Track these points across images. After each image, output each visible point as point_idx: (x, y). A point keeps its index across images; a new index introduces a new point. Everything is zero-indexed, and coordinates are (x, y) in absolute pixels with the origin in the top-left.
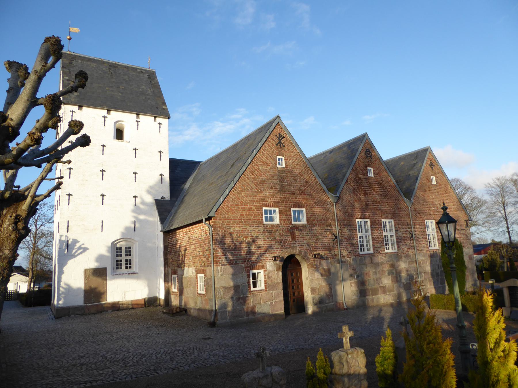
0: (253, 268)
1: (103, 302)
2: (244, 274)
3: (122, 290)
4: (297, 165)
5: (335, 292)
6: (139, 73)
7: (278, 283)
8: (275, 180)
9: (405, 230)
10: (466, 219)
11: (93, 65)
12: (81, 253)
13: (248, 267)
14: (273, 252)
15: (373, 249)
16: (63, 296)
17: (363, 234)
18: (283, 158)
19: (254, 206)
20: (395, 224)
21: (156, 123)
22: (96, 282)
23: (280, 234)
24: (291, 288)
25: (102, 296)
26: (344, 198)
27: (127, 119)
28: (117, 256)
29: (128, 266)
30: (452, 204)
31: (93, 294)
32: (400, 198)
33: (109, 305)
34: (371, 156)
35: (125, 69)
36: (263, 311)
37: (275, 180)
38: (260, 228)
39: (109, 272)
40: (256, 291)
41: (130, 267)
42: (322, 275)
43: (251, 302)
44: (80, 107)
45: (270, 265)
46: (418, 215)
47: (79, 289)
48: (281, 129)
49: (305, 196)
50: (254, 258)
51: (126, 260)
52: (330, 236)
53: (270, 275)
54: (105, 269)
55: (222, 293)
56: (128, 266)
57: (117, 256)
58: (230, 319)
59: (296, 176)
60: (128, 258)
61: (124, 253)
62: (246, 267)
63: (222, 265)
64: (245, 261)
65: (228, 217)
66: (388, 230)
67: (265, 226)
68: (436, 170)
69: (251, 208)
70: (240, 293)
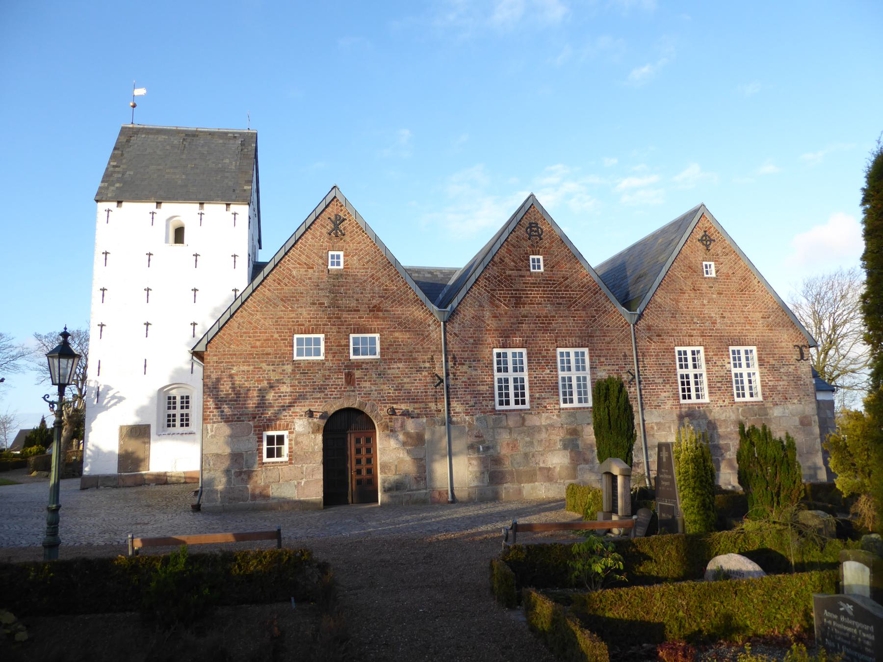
0: (267, 427)
1: (143, 472)
2: (253, 437)
3: (175, 457)
4: (368, 262)
5: (432, 472)
7: (313, 453)
8: (322, 289)
10: (801, 344)
11: (161, 138)
12: (115, 404)
13: (260, 426)
14: (307, 403)
15: (531, 401)
16: (89, 460)
17: (566, 374)
18: (341, 253)
20: (591, 357)
21: (229, 213)
22: (133, 445)
23: (324, 376)
24: (354, 462)
25: (142, 464)
26: (466, 313)
27: (184, 212)
28: (169, 408)
30: (759, 315)
31: (130, 461)
32: (609, 306)
33: (151, 477)
34: (539, 236)
35: (209, 137)
36: (283, 495)
37: (322, 289)
38: (285, 367)
39: (153, 430)
40: (273, 463)
41: (187, 425)
42: (404, 444)
43: (260, 479)
44: (119, 203)
45: (301, 425)
46: (655, 339)
47: (111, 453)
48: (342, 206)
49: (381, 314)
50: (270, 413)
51: (182, 415)
53: (300, 439)
54: (149, 426)
55: (211, 463)
57: (169, 408)
58: (221, 502)
59: (365, 281)
61: (178, 405)
62: (255, 427)
63: (214, 423)
65: (229, 351)
66: (510, 366)
69: (272, 336)
70: (240, 466)
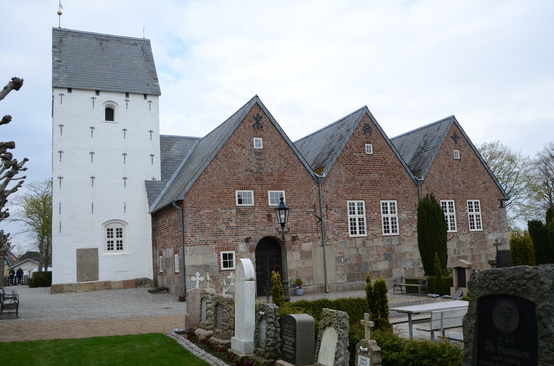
6: (133, 45)
9: (411, 212)
10: (502, 198)
13: (219, 248)
19: (227, 189)
28: (108, 237)
29: (120, 247)
51: (118, 242)
52: (313, 219)
56: (120, 247)
60: (119, 239)
62: (216, 248)
63: (191, 246)
64: (215, 243)
67: (238, 210)
68: (461, 142)
69: (223, 191)
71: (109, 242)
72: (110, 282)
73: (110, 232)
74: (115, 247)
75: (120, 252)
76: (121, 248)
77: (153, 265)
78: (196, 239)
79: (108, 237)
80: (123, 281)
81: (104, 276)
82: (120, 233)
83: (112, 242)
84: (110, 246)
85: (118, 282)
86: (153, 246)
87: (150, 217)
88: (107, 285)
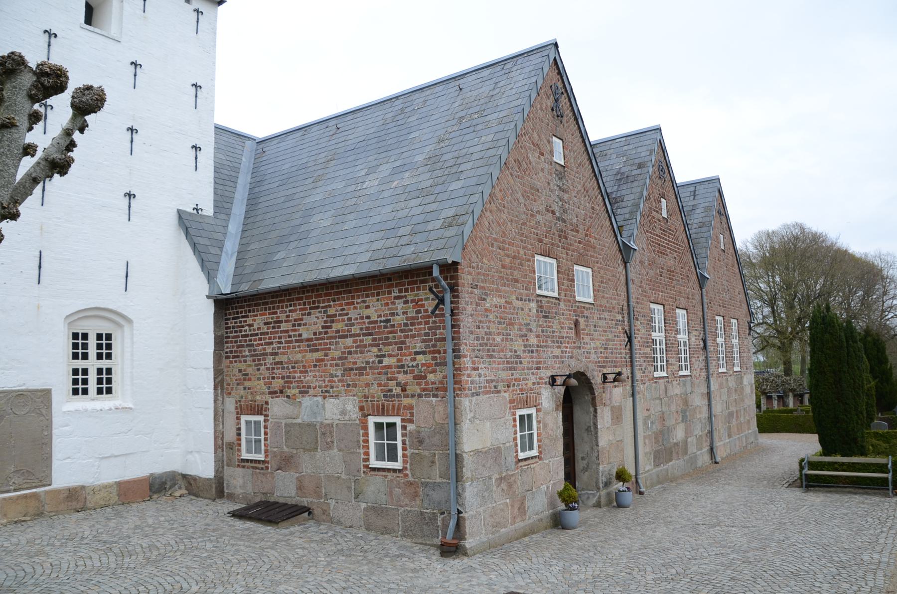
29: (104, 386)
60: (104, 364)
62: (511, 401)
71: (75, 372)
72: (83, 488)
73: (79, 341)
74: (92, 386)
75: (105, 403)
76: (109, 391)
77: (216, 438)
78: (480, 376)
79: (75, 356)
80: (119, 484)
81: (65, 473)
82: (105, 344)
83: (85, 371)
84: (79, 388)
85: (105, 487)
86: (215, 388)
87: (209, 308)
88: (75, 499)
